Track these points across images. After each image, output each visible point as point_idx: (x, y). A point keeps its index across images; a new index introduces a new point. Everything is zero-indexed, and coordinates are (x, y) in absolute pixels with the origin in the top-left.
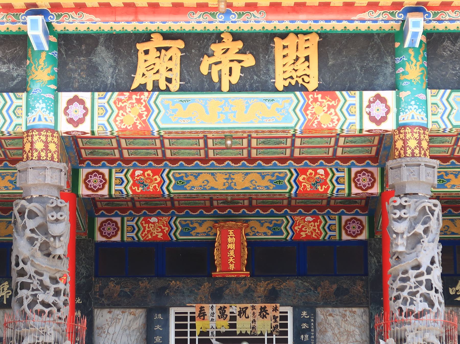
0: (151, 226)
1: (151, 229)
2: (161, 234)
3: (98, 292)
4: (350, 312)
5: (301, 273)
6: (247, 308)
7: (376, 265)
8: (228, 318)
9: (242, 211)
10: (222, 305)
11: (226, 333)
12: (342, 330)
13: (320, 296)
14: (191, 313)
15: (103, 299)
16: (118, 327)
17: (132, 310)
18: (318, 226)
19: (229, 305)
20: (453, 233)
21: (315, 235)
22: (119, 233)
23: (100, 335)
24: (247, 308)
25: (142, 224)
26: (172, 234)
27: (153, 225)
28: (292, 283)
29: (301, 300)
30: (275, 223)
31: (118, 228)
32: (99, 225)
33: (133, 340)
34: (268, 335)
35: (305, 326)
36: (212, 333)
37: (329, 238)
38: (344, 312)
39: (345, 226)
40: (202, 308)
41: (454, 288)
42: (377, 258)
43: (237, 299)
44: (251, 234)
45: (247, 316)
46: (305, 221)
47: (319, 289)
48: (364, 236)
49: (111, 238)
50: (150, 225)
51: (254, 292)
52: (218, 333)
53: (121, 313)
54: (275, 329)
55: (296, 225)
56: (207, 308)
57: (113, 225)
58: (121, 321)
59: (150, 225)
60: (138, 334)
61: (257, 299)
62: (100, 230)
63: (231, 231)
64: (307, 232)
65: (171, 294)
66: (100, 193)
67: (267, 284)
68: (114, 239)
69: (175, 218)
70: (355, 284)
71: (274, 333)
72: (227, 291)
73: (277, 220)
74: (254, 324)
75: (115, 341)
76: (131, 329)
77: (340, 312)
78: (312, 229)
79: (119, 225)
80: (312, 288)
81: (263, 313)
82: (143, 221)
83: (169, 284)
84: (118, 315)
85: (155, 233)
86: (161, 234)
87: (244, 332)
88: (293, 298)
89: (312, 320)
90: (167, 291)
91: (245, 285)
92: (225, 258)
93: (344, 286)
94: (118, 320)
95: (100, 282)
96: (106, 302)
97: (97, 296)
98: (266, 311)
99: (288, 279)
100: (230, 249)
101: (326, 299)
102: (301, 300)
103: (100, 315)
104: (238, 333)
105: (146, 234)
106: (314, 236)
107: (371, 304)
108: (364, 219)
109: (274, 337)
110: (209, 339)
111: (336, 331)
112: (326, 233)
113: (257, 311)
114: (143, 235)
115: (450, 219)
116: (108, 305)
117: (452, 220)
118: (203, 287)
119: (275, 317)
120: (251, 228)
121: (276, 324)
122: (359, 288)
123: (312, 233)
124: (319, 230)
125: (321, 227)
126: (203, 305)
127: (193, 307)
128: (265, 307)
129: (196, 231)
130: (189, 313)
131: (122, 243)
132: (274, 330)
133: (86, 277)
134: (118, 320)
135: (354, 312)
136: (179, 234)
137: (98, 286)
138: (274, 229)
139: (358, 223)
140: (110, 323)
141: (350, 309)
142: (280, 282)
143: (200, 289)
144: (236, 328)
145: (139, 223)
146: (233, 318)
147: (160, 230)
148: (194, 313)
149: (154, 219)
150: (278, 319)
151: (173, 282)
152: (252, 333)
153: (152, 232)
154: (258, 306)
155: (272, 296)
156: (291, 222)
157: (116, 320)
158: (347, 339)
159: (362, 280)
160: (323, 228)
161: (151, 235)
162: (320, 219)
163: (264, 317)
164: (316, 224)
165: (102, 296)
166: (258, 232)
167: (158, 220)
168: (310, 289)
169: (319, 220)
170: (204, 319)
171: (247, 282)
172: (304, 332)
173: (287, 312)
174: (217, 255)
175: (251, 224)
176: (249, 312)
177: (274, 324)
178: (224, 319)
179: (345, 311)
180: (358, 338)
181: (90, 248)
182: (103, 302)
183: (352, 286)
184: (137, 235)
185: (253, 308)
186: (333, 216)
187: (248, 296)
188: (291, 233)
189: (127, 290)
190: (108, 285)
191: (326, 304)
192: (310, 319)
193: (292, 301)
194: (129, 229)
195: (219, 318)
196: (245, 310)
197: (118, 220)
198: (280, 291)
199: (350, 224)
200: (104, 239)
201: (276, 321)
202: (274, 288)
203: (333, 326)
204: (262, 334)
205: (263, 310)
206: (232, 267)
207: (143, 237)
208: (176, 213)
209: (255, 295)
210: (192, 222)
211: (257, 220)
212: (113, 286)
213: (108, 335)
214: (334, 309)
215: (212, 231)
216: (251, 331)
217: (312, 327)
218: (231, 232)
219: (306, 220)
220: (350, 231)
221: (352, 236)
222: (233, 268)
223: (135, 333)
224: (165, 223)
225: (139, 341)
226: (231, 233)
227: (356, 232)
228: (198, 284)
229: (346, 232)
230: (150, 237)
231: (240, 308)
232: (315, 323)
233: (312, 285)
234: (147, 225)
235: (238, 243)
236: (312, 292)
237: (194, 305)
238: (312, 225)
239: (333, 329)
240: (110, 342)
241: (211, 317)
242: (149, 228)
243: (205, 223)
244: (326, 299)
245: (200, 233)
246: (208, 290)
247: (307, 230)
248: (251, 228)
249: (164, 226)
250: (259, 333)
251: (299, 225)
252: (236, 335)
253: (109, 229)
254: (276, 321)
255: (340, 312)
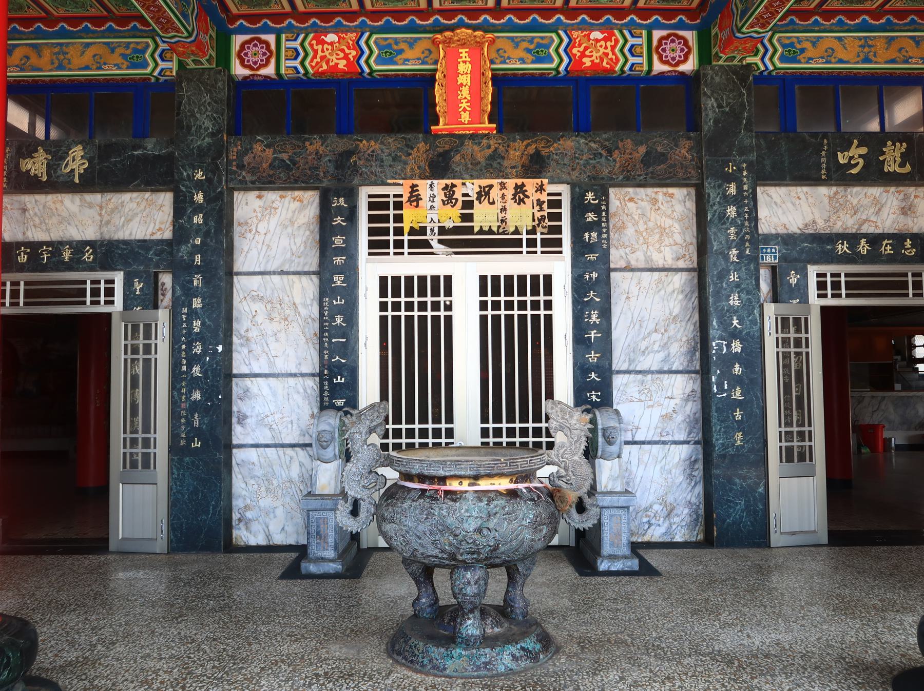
0: (327, 49)
1: (327, 53)
2: (344, 62)
3: (235, 160)
4: (665, 194)
5: (582, 127)
6: (491, 186)
7: (715, 111)
8: (460, 204)
9: (482, 18)
10: (449, 182)
11: (456, 230)
12: (651, 224)
13: (618, 165)
14: (395, 196)
15: (244, 173)
16: (274, 221)
17: (297, 193)
18: (613, 48)
19: (461, 181)
20: (841, 61)
21: (607, 63)
22: (273, 61)
23: (243, 236)
24: (491, 186)
25: (311, 45)
26: (362, 62)
27: (330, 47)
28: (569, 144)
29: (585, 173)
30: (538, 43)
31: (271, 52)
32: (238, 48)
33: (298, 245)
34: (528, 233)
35: (591, 217)
36: (432, 230)
37: (631, 69)
38: (653, 196)
39: (657, 48)
40: (413, 186)
41: (846, 153)
42: (716, 100)
43: (476, 171)
44: (498, 61)
45: (491, 201)
46: (589, 39)
47: (616, 154)
48: (689, 66)
49: (258, 69)
50: (326, 46)
51: (503, 158)
52: (442, 231)
53: (279, 199)
54: (540, 223)
55: (574, 46)
56: (423, 186)
57: (262, 48)
58: (278, 211)
59: (326, 46)
60: (308, 233)
61: (509, 170)
62: (239, 56)
63: (463, 51)
64: (594, 58)
65: (361, 162)
66: (263, 72)
67: (527, 146)
68: (263, 72)
69: (367, 34)
70: (677, 145)
71: (539, 230)
72: (457, 158)
73: (542, 38)
74: (503, 215)
75: (268, 246)
76: (296, 225)
77: (647, 195)
78: (601, 53)
79: (273, 47)
80: (604, 153)
81: (520, 195)
82: (313, 39)
83: (357, 146)
84: (273, 202)
85: (334, 60)
86: (344, 62)
87: (486, 229)
88: (570, 169)
89: (604, 207)
90: (354, 158)
91: (489, 147)
92: (452, 102)
93: (659, 149)
94: (273, 210)
95: (239, 143)
96: (249, 178)
97: (234, 168)
98: (523, 192)
99: (562, 137)
100: (462, 85)
101: (628, 171)
102: (585, 173)
103: (244, 202)
104: (476, 229)
105: (317, 63)
106: (605, 64)
107: (707, 179)
108: (690, 36)
109: (539, 237)
110: (427, 240)
111: (642, 227)
112: (627, 60)
113: (510, 192)
114: (314, 64)
115: (836, 38)
116: (253, 182)
117: (840, 39)
118: (415, 150)
119: (540, 203)
120: (498, 51)
121: (542, 213)
122: (684, 151)
123: (602, 60)
124: (614, 53)
125: (617, 50)
126: (416, 182)
127: (399, 185)
128: (523, 185)
129: (404, 56)
130: (392, 196)
131: (278, 82)
132: (538, 225)
133: (213, 135)
134: (273, 210)
135: (671, 196)
136: (375, 61)
137: (235, 149)
138: (538, 52)
139: (680, 43)
140: (259, 215)
141: (665, 190)
142: (548, 141)
143: (410, 154)
144: (472, 221)
145: (306, 44)
146: (468, 205)
147: (342, 55)
148: (401, 196)
149: (331, 37)
150: (545, 206)
151: (364, 142)
152: (501, 230)
153: (329, 60)
154: (511, 183)
155: (535, 166)
156: (566, 40)
157: (270, 209)
158: (660, 241)
159: (689, 138)
160: (622, 50)
161: (327, 63)
162: (614, 35)
163: (521, 201)
164: (609, 44)
165: (241, 167)
166: (509, 58)
167: (339, 38)
168: (601, 154)
169: (613, 38)
170: (417, 206)
171: (492, 142)
172: (591, 227)
173: (560, 194)
174: (441, 95)
175: (499, 44)
176: (495, 193)
177: (538, 215)
178: (452, 207)
179: (656, 193)
180: (678, 238)
181: (220, 84)
182: (244, 177)
183: (671, 148)
184: (302, 63)
185: (503, 186)
186: (638, 31)
187: (493, 166)
188: (566, 60)
189: (285, 156)
190: (251, 148)
191: (630, 180)
192: (599, 205)
193: (569, 174)
194: (290, 53)
195: (444, 204)
196: (489, 190)
197: (271, 38)
198: (549, 157)
199: (666, 44)
200: (247, 72)
201: (541, 210)
202: (537, 152)
203: (636, 217)
204: (517, 232)
205: (520, 189)
206: (465, 117)
207: (313, 67)
208: (369, 23)
209: (506, 163)
210: (397, 41)
211: (508, 38)
212: (262, 151)
213: (257, 236)
214: (638, 190)
215: (432, 56)
216: (499, 227)
217: (604, 219)
218: (464, 52)
219: (592, 37)
220: (666, 57)
221: (671, 65)
222: (467, 119)
223: (301, 232)
224: (351, 42)
225: (308, 244)
226: (463, 55)
227: (677, 58)
228: (407, 146)
229: (660, 58)
230: (325, 67)
231: (480, 187)
232: (607, 211)
233: (604, 147)
234: (320, 47)
235: (477, 74)
236: (604, 158)
237: (401, 182)
238: (601, 46)
239: (636, 224)
240: (259, 246)
241: (430, 204)
242: (323, 51)
243: (419, 42)
244: (628, 171)
245: (409, 63)
246: (425, 156)
247: (594, 53)
248: (498, 51)
249: (349, 48)
250: (512, 229)
251: (580, 45)
252: (473, 234)
253: (255, 54)
254: (541, 210)
255: (647, 195)
